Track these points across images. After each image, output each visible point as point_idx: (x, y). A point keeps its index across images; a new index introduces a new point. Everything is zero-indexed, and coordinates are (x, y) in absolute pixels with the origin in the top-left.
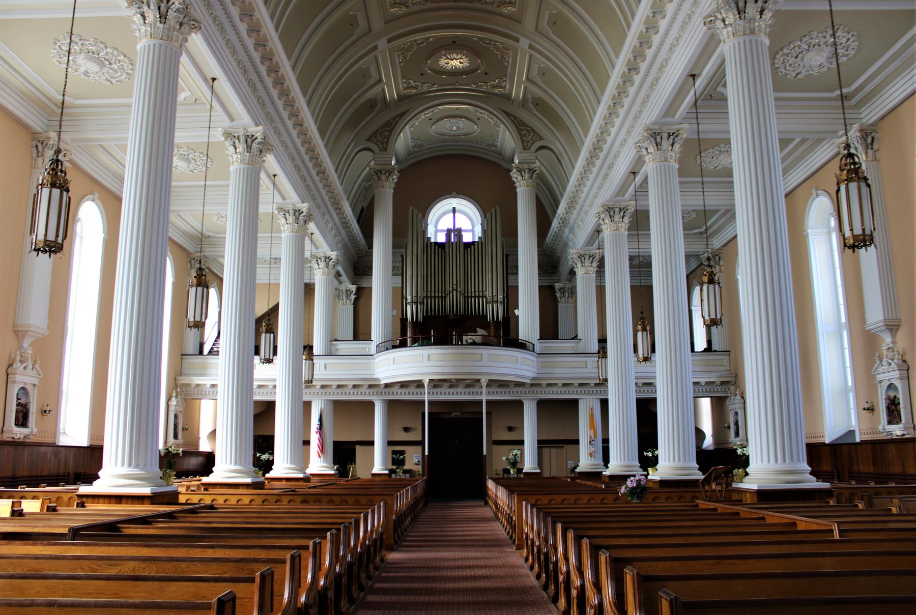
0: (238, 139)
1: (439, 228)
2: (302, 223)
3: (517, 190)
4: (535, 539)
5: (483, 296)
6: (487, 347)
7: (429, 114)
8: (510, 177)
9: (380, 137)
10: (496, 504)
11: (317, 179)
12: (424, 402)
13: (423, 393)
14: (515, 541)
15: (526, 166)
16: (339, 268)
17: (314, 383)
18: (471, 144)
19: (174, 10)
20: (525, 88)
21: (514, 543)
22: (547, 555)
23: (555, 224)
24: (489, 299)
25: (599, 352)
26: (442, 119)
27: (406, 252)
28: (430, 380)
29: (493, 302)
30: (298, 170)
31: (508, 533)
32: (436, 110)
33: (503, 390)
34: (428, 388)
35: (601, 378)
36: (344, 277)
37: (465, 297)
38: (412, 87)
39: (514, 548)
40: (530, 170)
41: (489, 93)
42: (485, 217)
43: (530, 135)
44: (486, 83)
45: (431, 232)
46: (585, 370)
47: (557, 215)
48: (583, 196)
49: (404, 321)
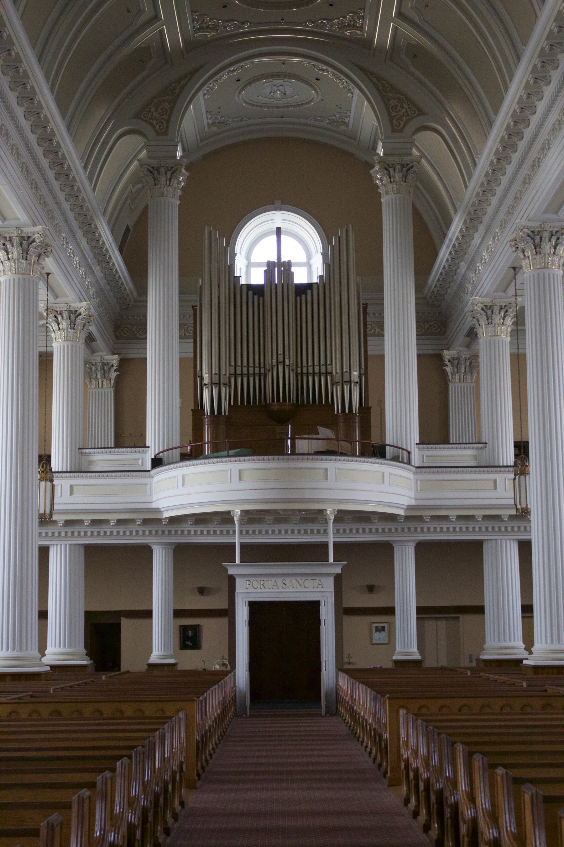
0: (10, 240)
1: (254, 260)
2: (33, 259)
3: (382, 200)
4: (421, 770)
5: (326, 373)
6: (334, 457)
7: (235, 71)
8: (370, 179)
9: (156, 111)
10: (352, 712)
11: (56, 185)
12: (233, 546)
13: (231, 532)
14: (386, 773)
15: (397, 160)
16: (93, 328)
17: (54, 518)
18: (306, 121)
19: (35, 246)
20: (395, 29)
21: (385, 777)
22: (440, 794)
23: (444, 254)
24: (337, 378)
25: (515, 465)
26: (257, 79)
27: (201, 300)
28: (242, 511)
29: (343, 382)
30: (35, 187)
31: (375, 759)
32: (248, 65)
33: (361, 527)
34: (240, 524)
35: (519, 506)
36: (100, 343)
37: (297, 374)
38: (208, 27)
39: (386, 782)
40: (403, 166)
41: (334, 36)
42: (330, 243)
43: (403, 108)
44: (331, 20)
45: (240, 269)
46: (493, 494)
47: (447, 241)
48: (490, 210)
49: (198, 412)
